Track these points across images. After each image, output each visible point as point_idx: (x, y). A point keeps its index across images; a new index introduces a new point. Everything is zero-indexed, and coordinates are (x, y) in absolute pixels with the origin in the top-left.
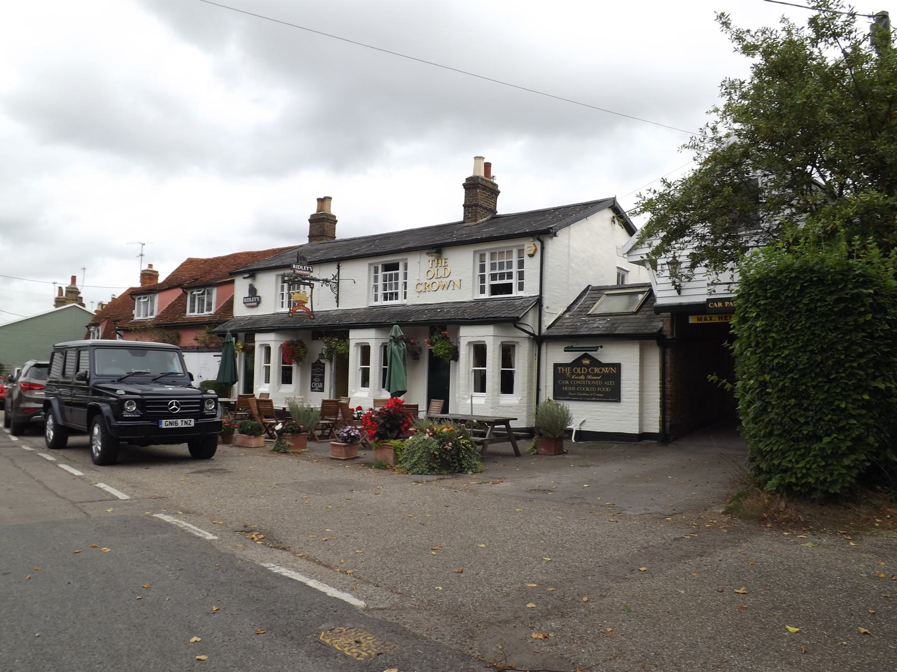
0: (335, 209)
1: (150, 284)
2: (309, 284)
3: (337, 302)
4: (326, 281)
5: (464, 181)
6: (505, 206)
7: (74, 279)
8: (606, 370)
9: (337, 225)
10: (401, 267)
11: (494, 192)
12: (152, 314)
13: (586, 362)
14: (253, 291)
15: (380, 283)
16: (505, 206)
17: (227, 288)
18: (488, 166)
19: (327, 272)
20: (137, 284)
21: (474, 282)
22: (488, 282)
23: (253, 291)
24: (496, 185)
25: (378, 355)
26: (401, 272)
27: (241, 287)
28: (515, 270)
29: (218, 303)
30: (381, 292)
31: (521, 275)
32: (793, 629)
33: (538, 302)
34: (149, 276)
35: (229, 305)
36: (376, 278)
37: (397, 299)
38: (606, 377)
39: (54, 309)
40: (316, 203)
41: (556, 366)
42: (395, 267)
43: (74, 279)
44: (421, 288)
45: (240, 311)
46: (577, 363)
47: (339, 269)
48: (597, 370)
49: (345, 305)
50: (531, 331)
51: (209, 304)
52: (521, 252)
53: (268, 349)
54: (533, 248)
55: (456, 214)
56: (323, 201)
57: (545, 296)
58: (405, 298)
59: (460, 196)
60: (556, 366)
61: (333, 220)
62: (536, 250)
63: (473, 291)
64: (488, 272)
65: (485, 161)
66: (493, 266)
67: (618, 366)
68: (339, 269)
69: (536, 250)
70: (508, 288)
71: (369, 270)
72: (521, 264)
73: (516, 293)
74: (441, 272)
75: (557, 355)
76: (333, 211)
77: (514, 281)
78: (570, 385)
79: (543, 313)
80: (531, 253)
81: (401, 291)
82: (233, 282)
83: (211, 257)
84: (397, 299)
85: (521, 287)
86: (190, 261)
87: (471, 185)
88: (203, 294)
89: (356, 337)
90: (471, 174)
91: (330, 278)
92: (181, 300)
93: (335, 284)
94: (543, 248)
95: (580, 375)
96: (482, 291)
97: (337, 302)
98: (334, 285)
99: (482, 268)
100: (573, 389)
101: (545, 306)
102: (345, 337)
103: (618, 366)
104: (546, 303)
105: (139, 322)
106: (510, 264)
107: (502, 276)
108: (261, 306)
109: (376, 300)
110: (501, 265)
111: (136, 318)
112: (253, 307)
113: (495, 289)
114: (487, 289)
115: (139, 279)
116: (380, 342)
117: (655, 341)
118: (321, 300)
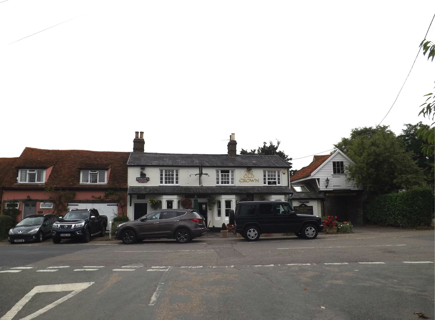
8: (309, 208)
9: (145, 145)
10: (230, 172)
13: (303, 206)
15: (220, 177)
22: (267, 181)
26: (230, 174)
28: (277, 177)
30: (220, 181)
31: (279, 179)
32: (323, 307)
36: (218, 175)
37: (173, 183)
38: (309, 210)
40: (135, 134)
42: (228, 172)
44: (241, 181)
46: (301, 206)
48: (306, 208)
52: (279, 173)
64: (267, 177)
66: (269, 176)
67: (312, 207)
70: (275, 183)
72: (279, 176)
73: (277, 185)
74: (250, 176)
77: (277, 180)
81: (230, 181)
83: (51, 149)
84: (173, 183)
85: (279, 183)
96: (265, 183)
99: (265, 176)
103: (312, 207)
106: (275, 176)
107: (272, 179)
108: (148, 182)
109: (218, 183)
110: (272, 176)
111: (19, 182)
113: (269, 183)
114: (267, 183)
117: (52, 240)
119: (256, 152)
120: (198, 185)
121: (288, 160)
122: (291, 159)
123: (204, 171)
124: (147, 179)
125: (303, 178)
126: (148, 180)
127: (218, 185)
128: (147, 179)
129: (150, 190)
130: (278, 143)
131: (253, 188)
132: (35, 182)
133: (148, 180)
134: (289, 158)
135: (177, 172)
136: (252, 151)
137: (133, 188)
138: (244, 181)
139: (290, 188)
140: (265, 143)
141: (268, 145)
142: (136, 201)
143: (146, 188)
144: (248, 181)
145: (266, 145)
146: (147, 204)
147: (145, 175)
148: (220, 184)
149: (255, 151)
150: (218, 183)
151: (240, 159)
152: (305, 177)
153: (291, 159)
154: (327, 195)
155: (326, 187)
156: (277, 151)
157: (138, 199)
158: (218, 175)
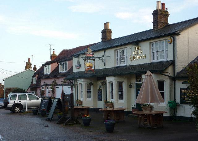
0: (110, 27)
1: (55, 59)
2: (93, 60)
3: (105, 66)
4: (99, 58)
5: (101, 31)
6: (114, 36)
7: (29, 59)
9: (101, 38)
11: (166, 15)
12: (66, 70)
14: (78, 62)
16: (114, 36)
17: (70, 61)
18: (163, 5)
19: (101, 54)
20: (49, 60)
21: (150, 55)
23: (78, 62)
24: (168, 12)
25: (117, 85)
27: (75, 60)
29: (68, 69)
33: (173, 63)
34: (53, 56)
35: (71, 69)
39: (25, 70)
41: (181, 89)
43: (29, 59)
45: (75, 70)
47: (105, 52)
49: (106, 67)
50: (168, 75)
51: (66, 68)
53: (112, 84)
54: (170, 40)
55: (150, 26)
56: (106, 24)
57: (176, 60)
58: (118, 64)
59: (151, 19)
60: (181, 89)
61: (110, 31)
62: (172, 41)
63: (115, 63)
65: (161, 2)
68: (105, 52)
69: (172, 41)
71: (115, 52)
75: (180, 85)
76: (110, 28)
78: (186, 98)
79: (176, 67)
80: (170, 42)
82: (72, 59)
86: (64, 51)
87: (155, 13)
88: (64, 64)
89: (109, 79)
90: (155, 9)
91: (101, 56)
92: (58, 67)
93: (104, 59)
94: (174, 40)
95: (190, 93)
97: (105, 66)
98: (103, 59)
100: (188, 99)
101: (176, 64)
102: (105, 79)
104: (176, 63)
105: (60, 73)
109: (64, 71)
112: (79, 68)
115: (50, 58)
116: (117, 81)
118: (99, 65)
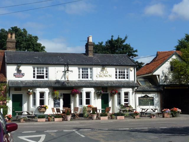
26: (89, 70)
36: (79, 72)
81: (89, 76)
108: (23, 77)
110: (122, 72)
119: (104, 44)
120: (63, 79)
121: (134, 52)
122: (136, 51)
123: (70, 68)
124: (22, 75)
125: (147, 74)
126: (23, 75)
127: (79, 79)
128: (22, 75)
129: (26, 84)
130: (126, 38)
131: (107, 82)
132: (44, 78)
133: (23, 75)
134: (134, 50)
135: (47, 68)
136: (99, 43)
137: (12, 82)
138: (100, 76)
139: (136, 82)
140: (112, 36)
141: (115, 38)
142: (13, 92)
143: (22, 82)
144: (103, 76)
145: (114, 39)
146: (22, 94)
147: (21, 71)
148: (81, 79)
149: (102, 43)
150: (79, 77)
151: (118, 68)
152: (148, 74)
153: (136, 51)
154: (165, 88)
155: (61, 79)
156: (124, 44)
157: (15, 90)
158: (79, 72)
